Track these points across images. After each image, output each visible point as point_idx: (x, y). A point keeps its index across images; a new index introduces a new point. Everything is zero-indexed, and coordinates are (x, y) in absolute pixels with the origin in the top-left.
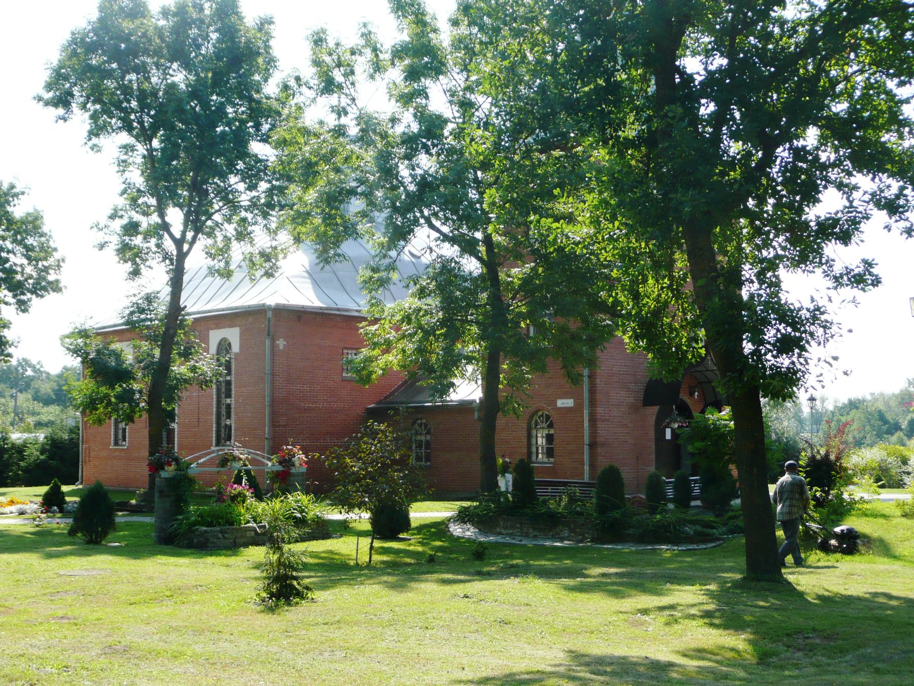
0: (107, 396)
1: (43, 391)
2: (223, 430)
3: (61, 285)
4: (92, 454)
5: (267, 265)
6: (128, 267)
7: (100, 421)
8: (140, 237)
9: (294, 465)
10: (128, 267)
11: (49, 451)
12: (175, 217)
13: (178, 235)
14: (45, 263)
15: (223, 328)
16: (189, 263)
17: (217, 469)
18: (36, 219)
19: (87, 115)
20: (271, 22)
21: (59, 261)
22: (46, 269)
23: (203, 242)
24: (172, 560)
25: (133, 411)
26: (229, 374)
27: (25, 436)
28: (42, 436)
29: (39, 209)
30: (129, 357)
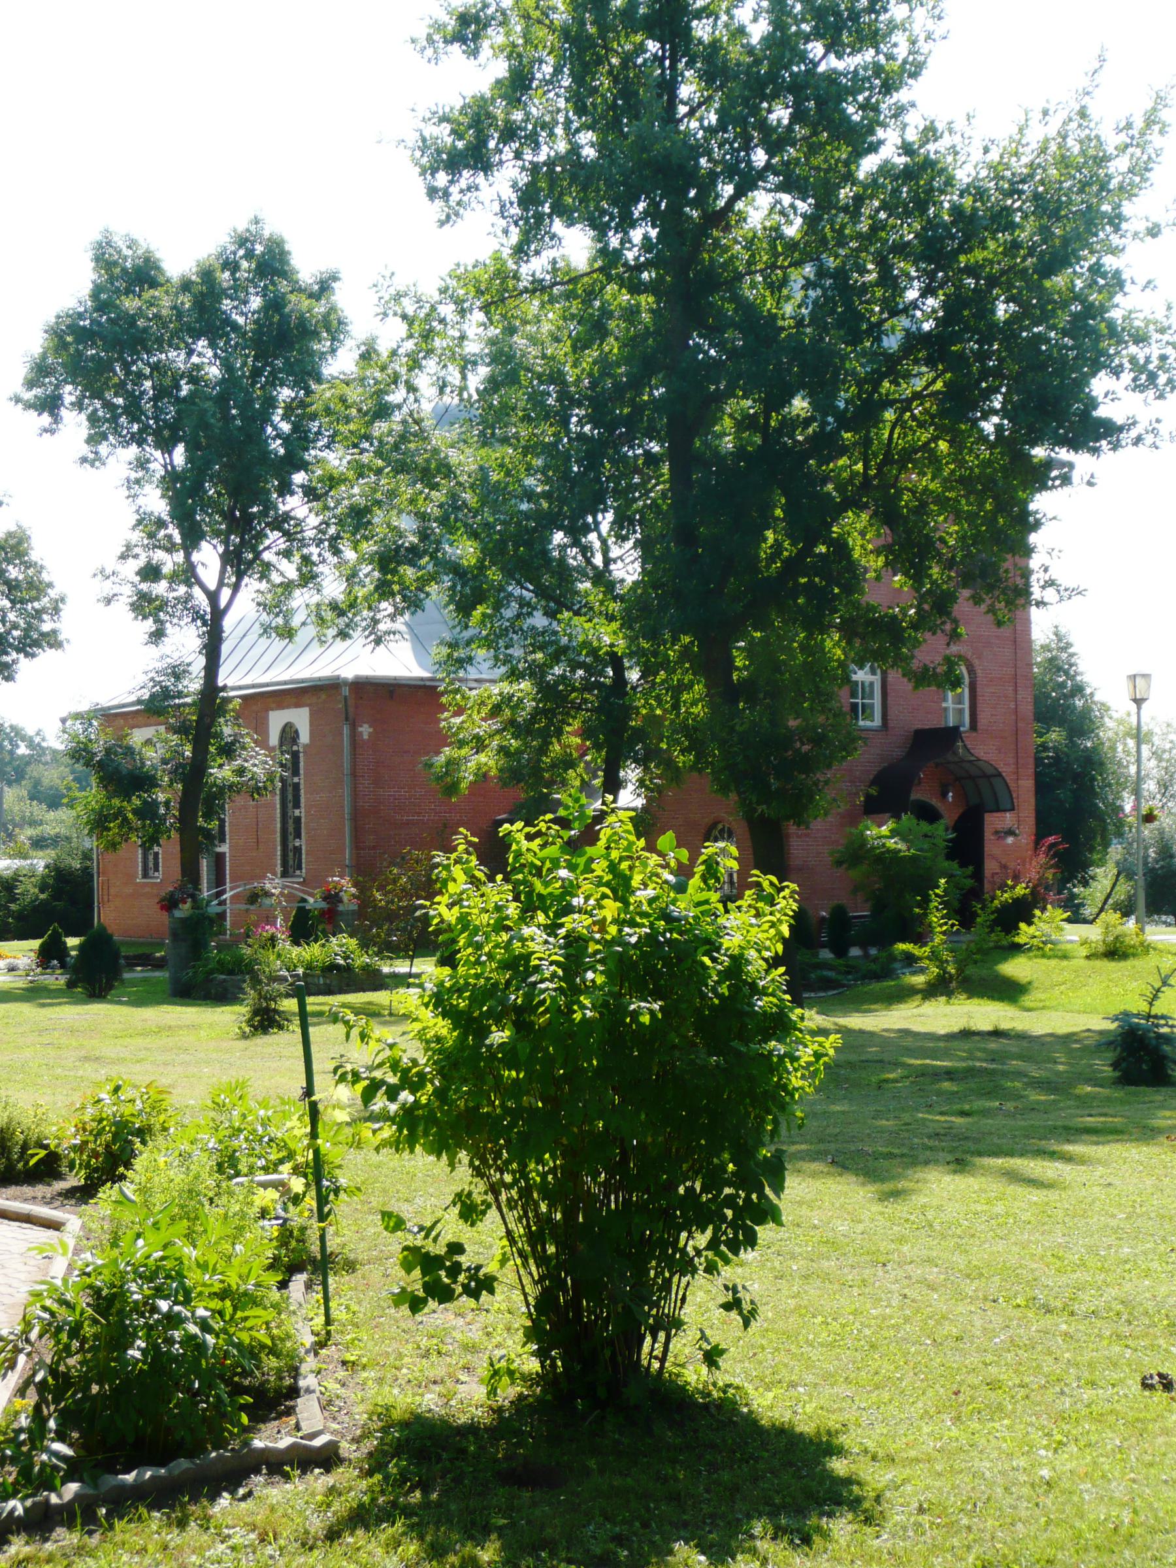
0: (120, 812)
1: (46, 782)
2: (291, 854)
3: (61, 637)
4: (112, 891)
5: (342, 621)
6: (149, 625)
7: (113, 846)
8: (164, 584)
9: (341, 901)
10: (149, 625)
11: (52, 886)
12: (208, 558)
13: (212, 586)
14: (36, 605)
15: (288, 707)
16: (228, 623)
17: (244, 907)
18: (20, 543)
19: (83, 417)
20: (335, 278)
21: (56, 601)
22: (38, 613)
23: (252, 586)
24: (179, 1008)
25: (157, 831)
26: (296, 772)
27: (17, 863)
28: (42, 864)
29: (25, 525)
30: (152, 756)
